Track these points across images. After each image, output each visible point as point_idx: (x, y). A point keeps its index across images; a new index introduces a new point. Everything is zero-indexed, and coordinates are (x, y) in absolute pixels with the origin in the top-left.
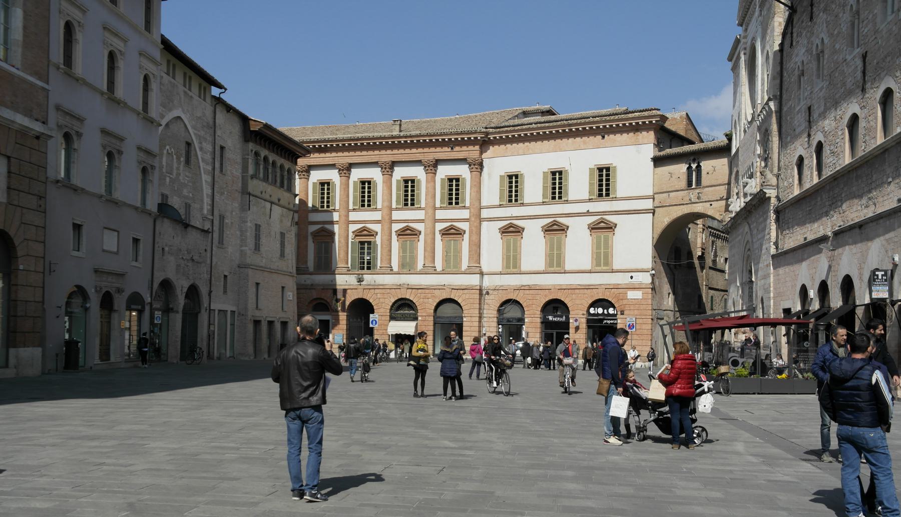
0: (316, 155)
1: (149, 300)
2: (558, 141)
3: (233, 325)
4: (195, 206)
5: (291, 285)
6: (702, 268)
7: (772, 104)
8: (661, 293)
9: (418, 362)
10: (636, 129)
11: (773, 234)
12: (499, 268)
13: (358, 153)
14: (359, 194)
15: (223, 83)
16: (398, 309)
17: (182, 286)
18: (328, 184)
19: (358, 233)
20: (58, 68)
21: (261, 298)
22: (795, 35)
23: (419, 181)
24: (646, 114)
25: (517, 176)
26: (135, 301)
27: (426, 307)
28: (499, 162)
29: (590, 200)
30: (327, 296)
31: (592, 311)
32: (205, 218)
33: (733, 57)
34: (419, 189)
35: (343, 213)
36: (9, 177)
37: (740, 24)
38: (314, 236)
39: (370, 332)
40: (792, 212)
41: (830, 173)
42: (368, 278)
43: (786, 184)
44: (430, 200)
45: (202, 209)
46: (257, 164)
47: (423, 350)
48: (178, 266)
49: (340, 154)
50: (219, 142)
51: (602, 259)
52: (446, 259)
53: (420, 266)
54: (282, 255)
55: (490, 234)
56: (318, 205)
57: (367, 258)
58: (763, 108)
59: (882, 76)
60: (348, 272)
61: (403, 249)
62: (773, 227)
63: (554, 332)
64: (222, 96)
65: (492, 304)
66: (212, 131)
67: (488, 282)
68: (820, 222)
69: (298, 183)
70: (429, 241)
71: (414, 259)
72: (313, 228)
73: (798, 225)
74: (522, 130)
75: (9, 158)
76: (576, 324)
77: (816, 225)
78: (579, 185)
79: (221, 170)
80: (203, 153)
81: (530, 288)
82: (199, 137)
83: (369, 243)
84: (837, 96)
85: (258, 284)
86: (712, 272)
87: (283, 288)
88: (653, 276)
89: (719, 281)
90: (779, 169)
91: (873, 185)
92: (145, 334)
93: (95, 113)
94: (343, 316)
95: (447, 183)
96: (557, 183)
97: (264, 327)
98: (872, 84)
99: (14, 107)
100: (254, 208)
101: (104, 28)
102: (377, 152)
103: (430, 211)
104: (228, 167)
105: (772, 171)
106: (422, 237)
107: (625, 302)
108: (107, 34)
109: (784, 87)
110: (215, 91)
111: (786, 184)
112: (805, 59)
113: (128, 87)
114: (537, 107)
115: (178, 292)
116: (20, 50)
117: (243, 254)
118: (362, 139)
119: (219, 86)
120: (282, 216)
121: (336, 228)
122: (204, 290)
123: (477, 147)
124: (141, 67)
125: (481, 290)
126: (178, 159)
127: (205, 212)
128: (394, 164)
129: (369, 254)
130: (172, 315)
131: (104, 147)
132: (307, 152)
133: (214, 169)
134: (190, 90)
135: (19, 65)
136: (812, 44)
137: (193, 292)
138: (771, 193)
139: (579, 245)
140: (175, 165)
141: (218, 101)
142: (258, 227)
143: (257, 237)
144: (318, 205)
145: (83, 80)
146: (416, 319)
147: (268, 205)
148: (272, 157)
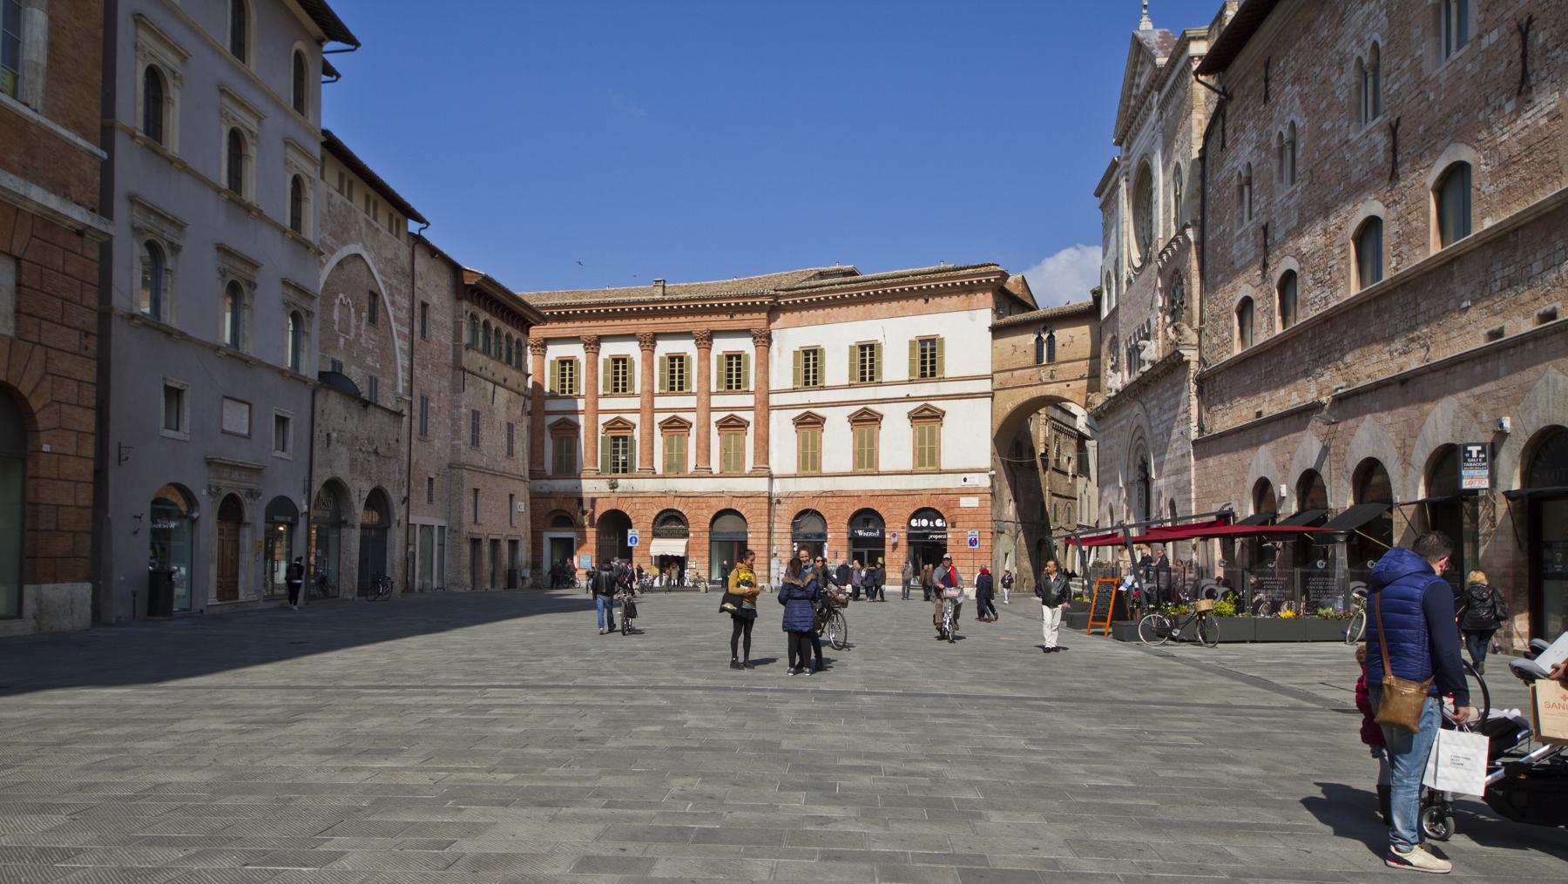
0: (555, 325)
1: (305, 508)
2: (869, 306)
3: (441, 545)
4: (385, 382)
5: (522, 491)
6: (1045, 469)
7: (1190, 233)
8: (1001, 500)
9: (739, 605)
10: (969, 289)
11: (1194, 412)
12: (849, 468)
13: (610, 322)
14: (610, 375)
15: (354, 31)
16: (663, 523)
17: (359, 489)
18: (571, 362)
19: (610, 426)
20: (133, 136)
21: (481, 509)
22: (1229, 132)
23: (689, 358)
24: (983, 270)
25: (815, 352)
26: (281, 508)
27: (699, 520)
28: (791, 336)
29: (910, 382)
30: (571, 507)
31: (914, 523)
32: (399, 399)
33: (1106, 192)
34: (689, 369)
35: (590, 399)
36: (18, 292)
37: (1119, 143)
38: (552, 428)
39: (627, 554)
40: (1214, 385)
41: (1313, 314)
42: (623, 484)
43: (1215, 340)
44: (703, 382)
45: (395, 386)
46: (474, 330)
47: (748, 583)
48: (353, 461)
49: (586, 324)
50: (420, 297)
51: (927, 457)
52: (725, 458)
53: (691, 467)
54: (510, 452)
55: (782, 427)
56: (557, 390)
57: (622, 458)
58: (1169, 245)
59: (1439, 146)
60: (598, 476)
61: (668, 445)
62: (1194, 402)
63: (865, 551)
64: (423, 233)
65: (785, 514)
66: (409, 280)
67: (779, 487)
68: (1291, 387)
69: (530, 360)
70: (703, 435)
71: (683, 458)
72: (550, 420)
73: (1242, 395)
74: (822, 292)
75: (18, 260)
76: (894, 540)
77: (1282, 392)
78: (896, 363)
79: (423, 335)
80: (395, 309)
81: (833, 494)
82: (390, 287)
83: (625, 438)
84: (1328, 199)
85: (476, 491)
86: (1055, 474)
87: (511, 496)
88: (992, 477)
89: (1062, 485)
90: (1202, 321)
91: (1421, 318)
92: (299, 559)
93: (205, 222)
94: (591, 533)
95: (725, 362)
96: (867, 359)
97: (486, 548)
98: (1414, 163)
99: (26, 173)
100: (470, 390)
101: (222, 91)
102: (634, 321)
103: (704, 397)
104: (433, 332)
105: (1190, 325)
106: (693, 431)
107: (956, 511)
108: (226, 101)
109: (1209, 208)
110: (413, 226)
111: (1215, 340)
112: (1254, 161)
113: (265, 184)
114: (838, 267)
115: (354, 497)
116: (40, 81)
117: (455, 450)
118: (614, 304)
119: (419, 219)
120: (510, 401)
121: (582, 419)
122: (395, 496)
123: (764, 315)
124: (286, 162)
125: (770, 498)
126: (358, 313)
127: (400, 390)
128: (656, 337)
129: (624, 452)
130: (344, 531)
131: (223, 273)
132: (544, 320)
133: (412, 332)
134: (375, 219)
135: (39, 105)
136: (1269, 134)
137: (377, 500)
138: (1191, 355)
139: (896, 439)
140: (353, 322)
141: (418, 240)
142: (476, 415)
143: (476, 429)
144: (557, 390)
145: (180, 162)
146: (686, 535)
147: (490, 386)
148: (495, 323)
